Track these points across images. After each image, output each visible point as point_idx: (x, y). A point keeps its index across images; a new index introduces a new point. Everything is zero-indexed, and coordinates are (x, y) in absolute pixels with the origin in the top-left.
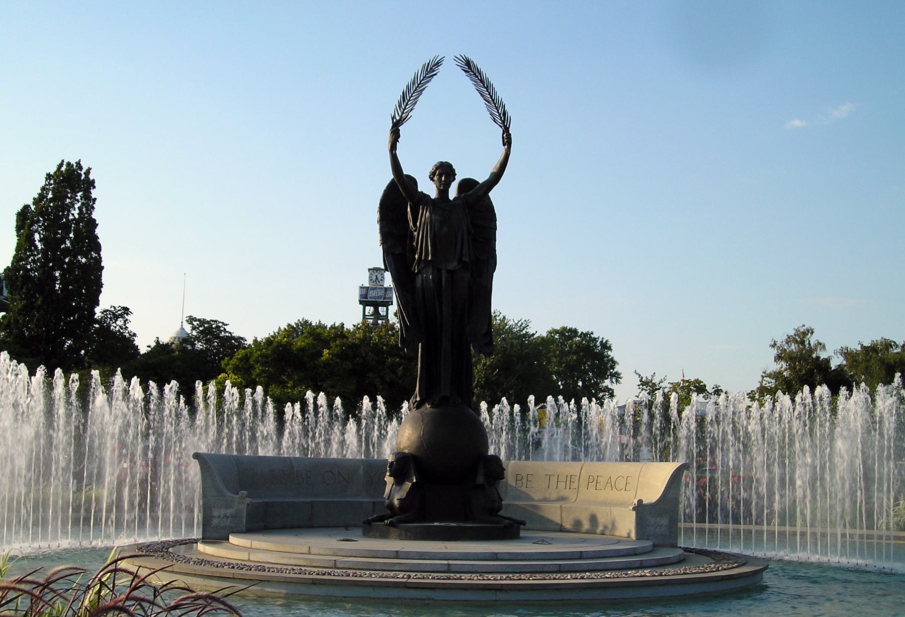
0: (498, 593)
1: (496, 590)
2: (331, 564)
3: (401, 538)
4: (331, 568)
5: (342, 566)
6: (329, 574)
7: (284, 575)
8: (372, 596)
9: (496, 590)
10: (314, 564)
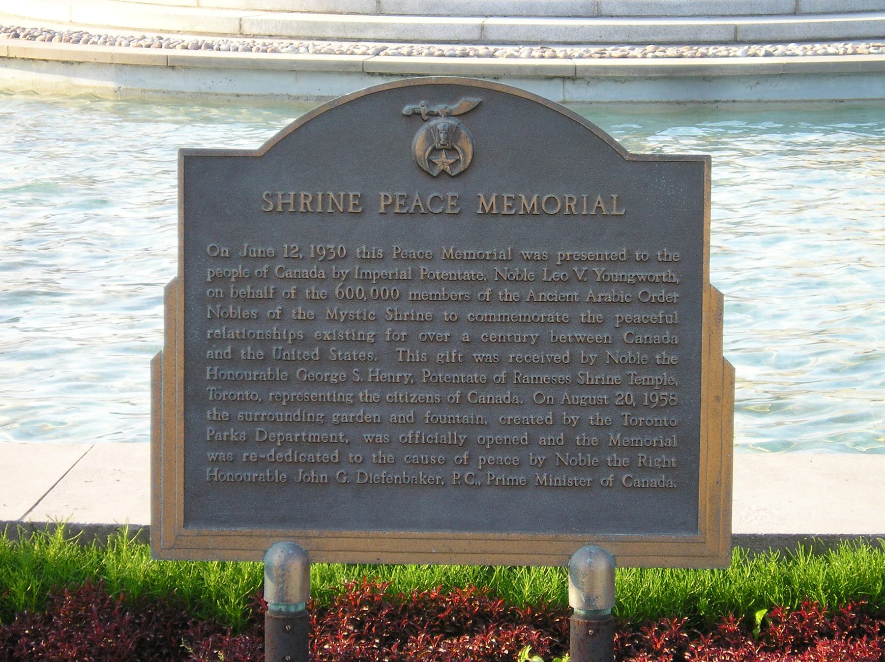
0: (569, 85)
1: (564, 78)
2: (233, 28)
3: (518, 25)
4: (233, 35)
5: (255, 31)
6: (209, 47)
7: (116, 50)
8: (294, 92)
9: (564, 78)
10: (199, 28)
